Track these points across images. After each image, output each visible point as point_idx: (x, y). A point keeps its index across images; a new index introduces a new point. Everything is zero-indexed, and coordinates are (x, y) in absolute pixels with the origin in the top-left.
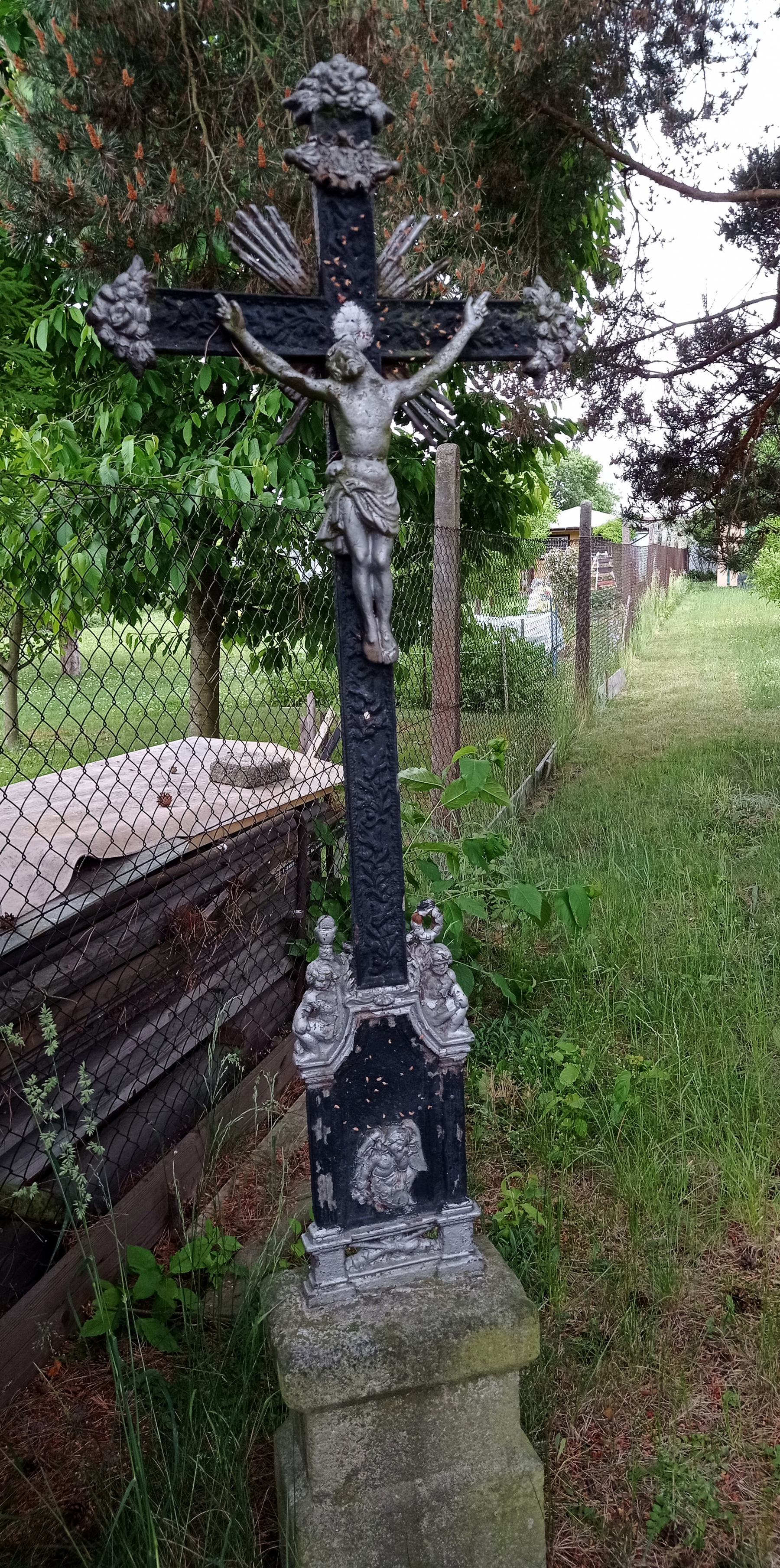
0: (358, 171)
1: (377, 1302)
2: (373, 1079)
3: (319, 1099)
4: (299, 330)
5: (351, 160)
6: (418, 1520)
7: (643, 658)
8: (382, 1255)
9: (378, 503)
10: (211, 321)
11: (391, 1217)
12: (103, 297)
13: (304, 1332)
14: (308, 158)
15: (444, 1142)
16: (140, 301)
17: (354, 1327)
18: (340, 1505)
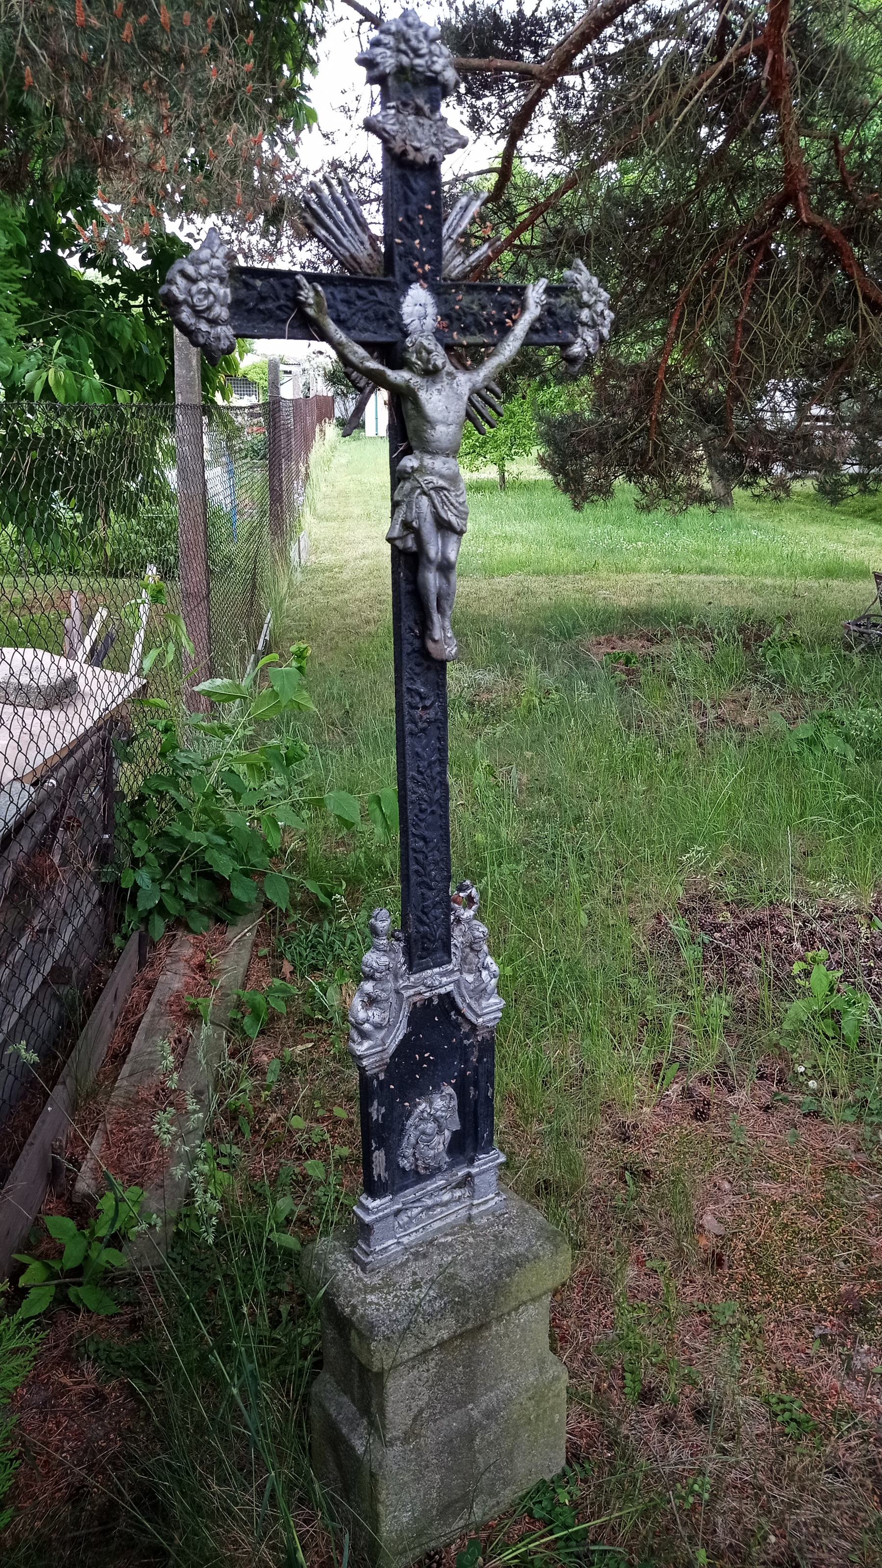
0: (433, 144)
1: (425, 1256)
2: (422, 1056)
3: (375, 1082)
4: (371, 313)
5: (426, 131)
6: (473, 1440)
7: (321, 518)
8: (422, 1212)
9: (454, 501)
10: (289, 304)
11: (430, 1177)
12: (184, 274)
13: (371, 1298)
14: (388, 127)
15: (476, 1102)
16: (222, 281)
17: (416, 1285)
18: (409, 1444)
